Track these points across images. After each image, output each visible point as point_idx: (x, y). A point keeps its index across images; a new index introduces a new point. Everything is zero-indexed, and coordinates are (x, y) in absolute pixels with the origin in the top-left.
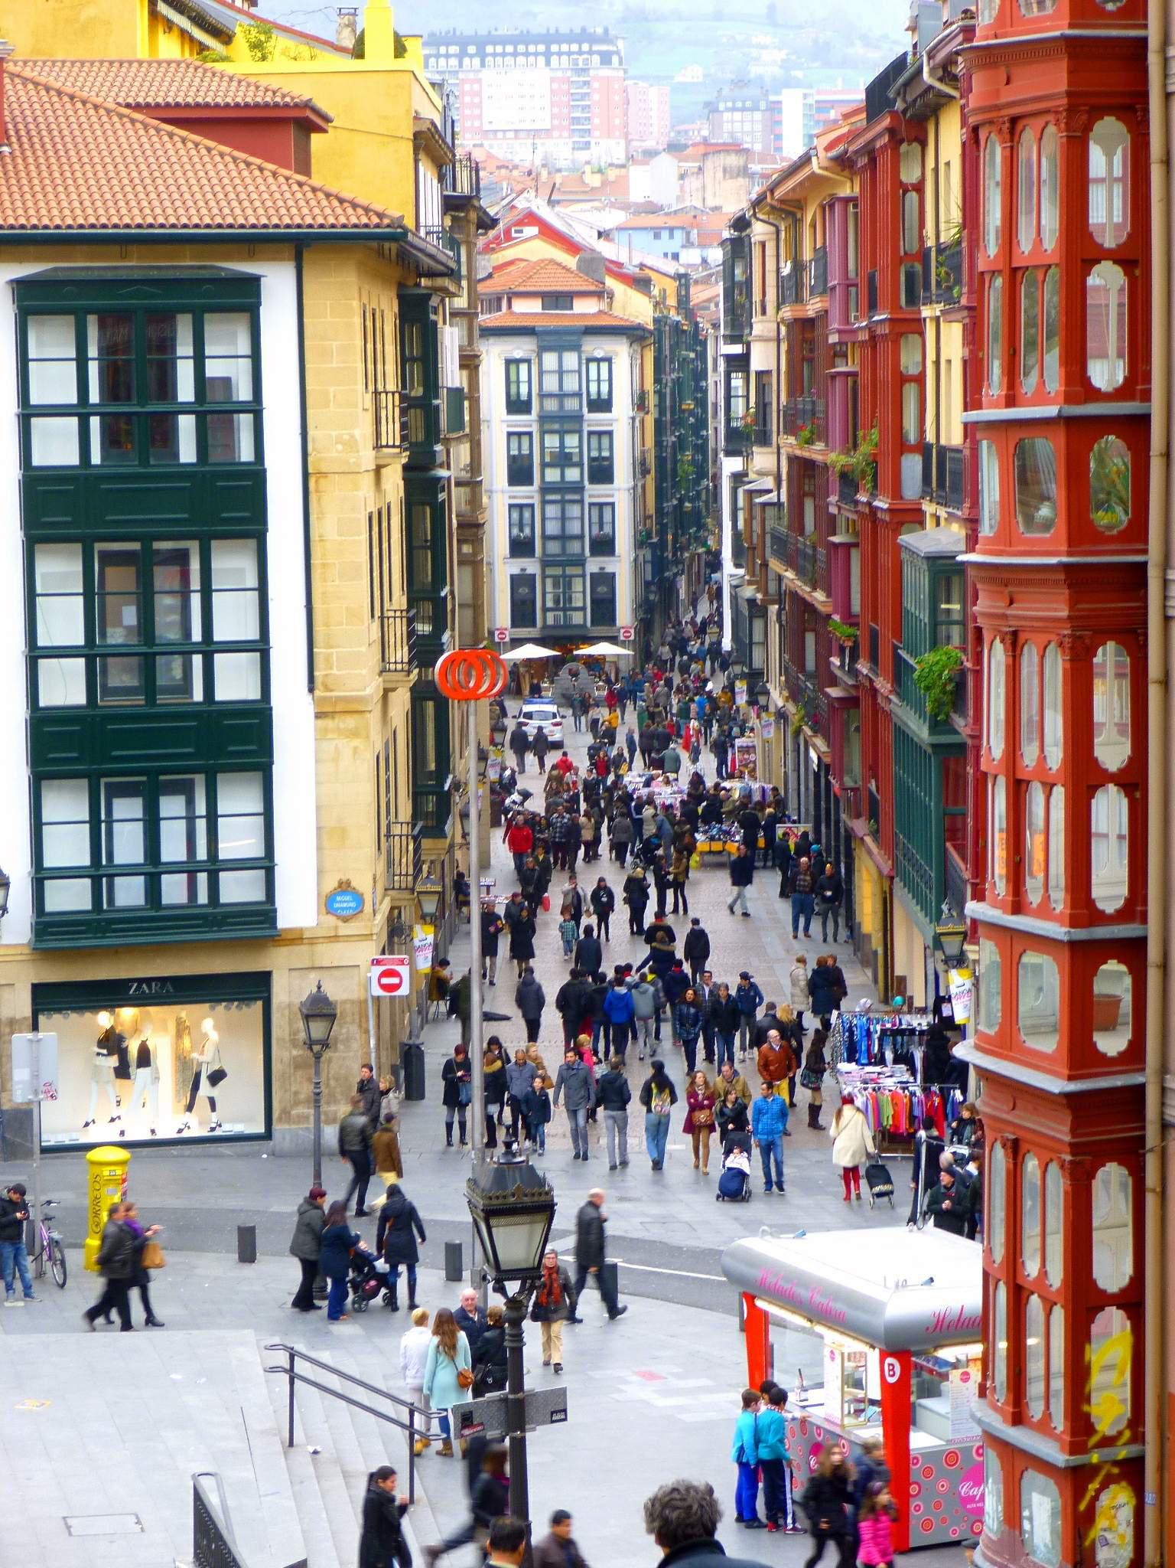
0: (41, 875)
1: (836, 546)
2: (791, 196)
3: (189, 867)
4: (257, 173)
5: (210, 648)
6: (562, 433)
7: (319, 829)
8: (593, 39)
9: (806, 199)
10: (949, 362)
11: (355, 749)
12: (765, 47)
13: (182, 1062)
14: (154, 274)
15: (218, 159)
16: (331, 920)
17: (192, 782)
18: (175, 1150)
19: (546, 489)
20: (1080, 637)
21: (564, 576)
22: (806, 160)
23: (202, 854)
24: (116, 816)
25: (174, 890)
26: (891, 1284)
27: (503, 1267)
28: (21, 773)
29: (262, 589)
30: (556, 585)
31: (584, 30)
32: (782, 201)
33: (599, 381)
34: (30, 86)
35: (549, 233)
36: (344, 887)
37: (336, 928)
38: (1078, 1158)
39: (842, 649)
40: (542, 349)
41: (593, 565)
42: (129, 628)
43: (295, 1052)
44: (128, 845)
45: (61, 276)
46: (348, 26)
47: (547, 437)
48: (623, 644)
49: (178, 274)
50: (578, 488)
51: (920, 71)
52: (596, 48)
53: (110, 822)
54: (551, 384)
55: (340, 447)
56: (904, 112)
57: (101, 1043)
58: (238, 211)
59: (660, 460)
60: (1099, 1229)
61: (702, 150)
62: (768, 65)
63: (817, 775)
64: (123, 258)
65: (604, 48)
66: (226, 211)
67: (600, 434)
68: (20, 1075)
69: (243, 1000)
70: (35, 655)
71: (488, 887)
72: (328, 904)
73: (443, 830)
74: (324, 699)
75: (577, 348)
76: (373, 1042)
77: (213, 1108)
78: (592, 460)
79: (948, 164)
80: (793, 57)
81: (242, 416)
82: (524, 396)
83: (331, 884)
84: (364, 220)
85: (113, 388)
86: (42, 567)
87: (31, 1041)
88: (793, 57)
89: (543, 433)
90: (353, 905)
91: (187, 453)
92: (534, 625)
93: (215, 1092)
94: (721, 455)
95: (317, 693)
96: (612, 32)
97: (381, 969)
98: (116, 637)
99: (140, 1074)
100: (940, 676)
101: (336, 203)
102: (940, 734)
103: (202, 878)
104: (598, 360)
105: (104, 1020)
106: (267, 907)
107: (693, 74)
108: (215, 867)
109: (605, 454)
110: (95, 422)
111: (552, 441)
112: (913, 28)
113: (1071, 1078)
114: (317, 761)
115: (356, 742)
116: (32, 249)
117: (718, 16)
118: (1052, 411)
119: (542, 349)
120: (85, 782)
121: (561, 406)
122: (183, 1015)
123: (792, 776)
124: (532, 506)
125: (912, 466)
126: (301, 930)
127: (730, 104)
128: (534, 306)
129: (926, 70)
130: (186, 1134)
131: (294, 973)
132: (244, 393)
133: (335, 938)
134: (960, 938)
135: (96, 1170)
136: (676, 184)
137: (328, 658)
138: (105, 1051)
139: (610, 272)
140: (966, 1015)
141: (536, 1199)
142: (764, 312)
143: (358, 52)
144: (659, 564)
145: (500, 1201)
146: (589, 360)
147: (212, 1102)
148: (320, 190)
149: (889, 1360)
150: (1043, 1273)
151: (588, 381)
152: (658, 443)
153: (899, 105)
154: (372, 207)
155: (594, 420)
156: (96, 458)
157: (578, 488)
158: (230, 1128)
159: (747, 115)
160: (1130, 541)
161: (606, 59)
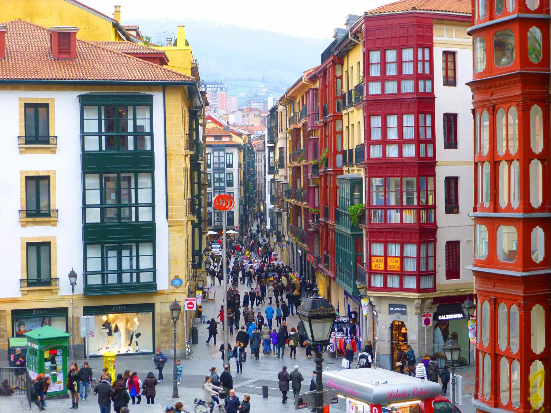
0: (86, 273)
1: (310, 188)
2: (292, 96)
3: (131, 272)
4: (151, 66)
5: (137, 206)
6: (219, 173)
7: (169, 260)
8: (218, 84)
9: (296, 96)
10: (353, 125)
11: (180, 237)
12: (262, 88)
13: (128, 331)
14: (121, 94)
15: (140, 63)
16: (173, 287)
17: (131, 246)
18: (126, 357)
19: (215, 188)
20: (526, 102)
21: (220, 212)
22: (301, 80)
23: (134, 267)
24: (109, 256)
25: (126, 278)
26: (374, 383)
27: (315, 340)
28: (79, 242)
30: (218, 215)
31: (215, 81)
32: (289, 97)
33: (229, 159)
34: (83, 43)
35: (214, 121)
36: (177, 278)
37: (174, 290)
38: (526, 302)
39: (313, 216)
40: (214, 151)
42: (113, 200)
43: (162, 327)
44: (112, 265)
45: (94, 94)
46: (169, 44)
47: (215, 174)
48: (236, 231)
49: (129, 94)
50: (224, 188)
51: (347, 36)
52: (218, 86)
53: (107, 258)
54: (216, 160)
55: (176, 146)
56: (337, 55)
57: (103, 325)
58: (146, 76)
59: (245, 182)
60: (512, 337)
61: (248, 110)
62: (263, 92)
63: (301, 257)
64: (112, 89)
65: (221, 86)
66: (143, 76)
67: (230, 173)
68: (83, 329)
69: (146, 312)
70: (85, 207)
71: (208, 289)
72: (172, 283)
73: (201, 266)
74: (171, 221)
75: (223, 150)
76: (185, 324)
77: (137, 345)
78: (227, 181)
79: (352, 68)
80: (269, 90)
81: (147, 137)
82: (209, 164)
83: (173, 277)
84: (184, 79)
85: (109, 127)
87: (86, 318)
88: (269, 90)
89: (214, 173)
90: (179, 283)
91: (131, 147)
92: (211, 225)
93: (137, 340)
94: (267, 174)
95: (169, 219)
96: (223, 82)
97: (188, 302)
98: (109, 202)
99: (115, 335)
100: (357, 211)
101: (175, 75)
102: (355, 231)
103: (135, 275)
104: (229, 154)
105: (104, 318)
106: (154, 283)
107: (243, 95)
108: (138, 271)
109: (231, 179)
110: (103, 138)
111: (217, 175)
112: (335, 37)
113: (523, 271)
114: (169, 240)
115: (180, 234)
116: (85, 87)
117: (249, 80)
118: (514, 16)
119: (214, 151)
120: (99, 246)
121: (219, 166)
122: (128, 317)
123: (291, 260)
124: (211, 193)
125: (339, 157)
126: (164, 290)
127: (254, 101)
128: (212, 139)
129: (349, 35)
130: (129, 352)
131: (162, 304)
132: (148, 130)
133: (174, 293)
134: (365, 289)
135: (106, 359)
136: (242, 119)
137: (172, 209)
138: (105, 328)
139: (231, 132)
140: (367, 313)
141: (329, 312)
142: (282, 131)
143: (175, 44)
144: (245, 210)
145: (315, 313)
146: (227, 154)
147: (137, 342)
148: (170, 71)
149: (374, 408)
150: (509, 348)
151: (226, 159)
152: (244, 178)
153: (336, 53)
154: (186, 75)
155: (228, 170)
156: (104, 149)
157: (224, 188)
158: (142, 351)
159: (258, 104)
160: (542, 66)
161: (221, 89)
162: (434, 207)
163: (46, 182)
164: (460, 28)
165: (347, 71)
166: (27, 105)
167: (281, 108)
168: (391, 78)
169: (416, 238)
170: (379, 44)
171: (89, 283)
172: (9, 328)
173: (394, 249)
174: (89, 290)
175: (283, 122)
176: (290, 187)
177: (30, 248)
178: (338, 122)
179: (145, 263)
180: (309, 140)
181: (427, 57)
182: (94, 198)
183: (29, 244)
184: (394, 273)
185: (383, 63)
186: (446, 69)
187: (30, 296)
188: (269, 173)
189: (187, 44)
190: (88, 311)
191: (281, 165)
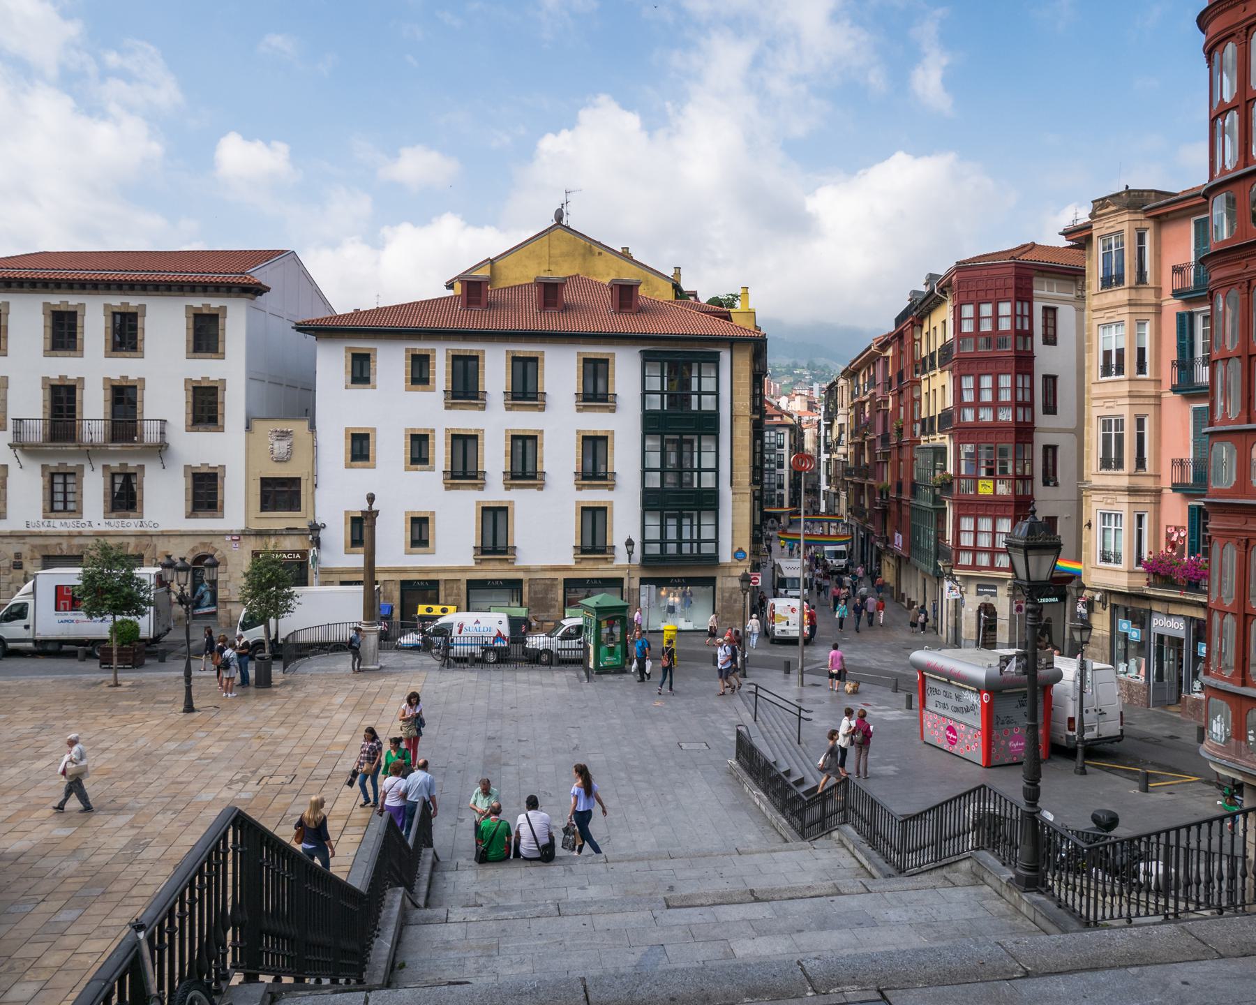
0: (644, 542)
3: (691, 541)
5: (700, 470)
10: (935, 390)
23: (695, 537)
25: (686, 549)
28: (639, 509)
29: (717, 452)
36: (740, 550)
41: (778, 492)
44: (672, 533)
50: (774, 470)
63: (862, 539)
72: (735, 555)
75: (774, 430)
79: (935, 328)
83: (736, 549)
86: (648, 443)
91: (694, 407)
103: (695, 545)
108: (700, 541)
125: (918, 427)
153: (915, 314)
157: (774, 470)
162: (1031, 478)
163: (603, 443)
164: (1061, 282)
165: (928, 334)
166: (586, 361)
167: (842, 382)
169: (1011, 511)
170: (972, 296)
171: (648, 552)
172: (561, 598)
173: (985, 524)
174: (647, 560)
175: (844, 397)
176: (851, 464)
177: (585, 512)
178: (916, 388)
179: (707, 533)
180: (878, 411)
181: (1026, 313)
182: (654, 460)
183: (584, 509)
184: (984, 550)
186: (1045, 326)
187: (584, 565)
188: (825, 452)
190: (643, 581)
191: (838, 442)
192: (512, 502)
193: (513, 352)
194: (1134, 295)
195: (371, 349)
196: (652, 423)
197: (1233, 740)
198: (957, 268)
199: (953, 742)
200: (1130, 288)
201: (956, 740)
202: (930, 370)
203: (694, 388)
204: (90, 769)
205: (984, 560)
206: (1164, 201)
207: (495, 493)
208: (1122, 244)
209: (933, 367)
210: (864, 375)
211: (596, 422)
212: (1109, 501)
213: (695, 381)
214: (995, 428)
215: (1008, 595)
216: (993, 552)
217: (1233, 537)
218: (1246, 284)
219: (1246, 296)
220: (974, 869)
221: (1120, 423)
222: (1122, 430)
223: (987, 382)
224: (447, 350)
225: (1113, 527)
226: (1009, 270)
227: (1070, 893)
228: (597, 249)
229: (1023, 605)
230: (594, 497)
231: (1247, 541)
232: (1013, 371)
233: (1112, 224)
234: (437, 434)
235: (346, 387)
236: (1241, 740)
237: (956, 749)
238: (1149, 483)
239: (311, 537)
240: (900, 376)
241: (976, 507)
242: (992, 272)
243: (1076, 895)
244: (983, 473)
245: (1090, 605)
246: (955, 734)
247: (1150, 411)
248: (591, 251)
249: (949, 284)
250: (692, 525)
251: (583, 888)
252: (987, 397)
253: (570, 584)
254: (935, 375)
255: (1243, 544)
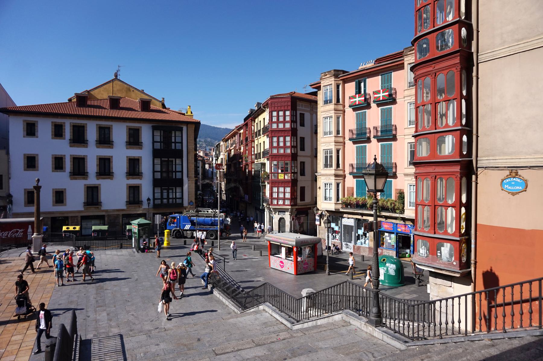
0: (154, 199)
3: (173, 198)
5: (176, 172)
23: (174, 197)
36: (191, 201)
72: (189, 203)
83: (190, 201)
91: (173, 147)
98: (164, 170)
103: (174, 200)
108: (176, 198)
113: (460, 158)
162: (297, 173)
168: (281, 122)
169: (290, 185)
173: (281, 189)
178: (253, 143)
179: (178, 195)
181: (295, 114)
182: (158, 168)
185: (278, 116)
189: (192, 113)
192: (100, 185)
193: (99, 124)
194: (336, 107)
195: (35, 121)
196: (156, 154)
197: (430, 256)
198: (271, 98)
199: (282, 267)
200: (335, 104)
201: (283, 266)
202: (259, 136)
203: (173, 140)
204: (17, 277)
205: (281, 202)
206: (346, 74)
207: (92, 180)
208: (332, 89)
209: (260, 135)
210: (231, 140)
211: (134, 153)
212: (327, 179)
213: (173, 138)
214: (284, 156)
215: (289, 214)
216: (284, 199)
217: (429, 175)
218: (434, 74)
219: (434, 79)
220: (344, 319)
221: (331, 152)
222: (332, 154)
223: (281, 139)
224: (70, 123)
225: (329, 188)
226: (289, 99)
227: (292, 313)
228: (132, 89)
229: (294, 218)
230: (134, 182)
231: (436, 176)
232: (291, 135)
233: (328, 81)
234: (66, 157)
235: (24, 137)
236: (434, 255)
237: (283, 269)
238: (341, 173)
239: (8, 200)
240: (247, 139)
241: (276, 183)
242: (283, 100)
243: (294, 314)
244: (280, 171)
245: (321, 216)
246: (283, 264)
247: (341, 147)
248: (129, 90)
249: (267, 104)
250: (173, 192)
251: (158, 345)
252: (281, 144)
253: (124, 216)
254: (260, 138)
255: (434, 178)
